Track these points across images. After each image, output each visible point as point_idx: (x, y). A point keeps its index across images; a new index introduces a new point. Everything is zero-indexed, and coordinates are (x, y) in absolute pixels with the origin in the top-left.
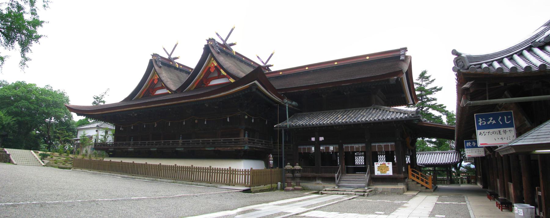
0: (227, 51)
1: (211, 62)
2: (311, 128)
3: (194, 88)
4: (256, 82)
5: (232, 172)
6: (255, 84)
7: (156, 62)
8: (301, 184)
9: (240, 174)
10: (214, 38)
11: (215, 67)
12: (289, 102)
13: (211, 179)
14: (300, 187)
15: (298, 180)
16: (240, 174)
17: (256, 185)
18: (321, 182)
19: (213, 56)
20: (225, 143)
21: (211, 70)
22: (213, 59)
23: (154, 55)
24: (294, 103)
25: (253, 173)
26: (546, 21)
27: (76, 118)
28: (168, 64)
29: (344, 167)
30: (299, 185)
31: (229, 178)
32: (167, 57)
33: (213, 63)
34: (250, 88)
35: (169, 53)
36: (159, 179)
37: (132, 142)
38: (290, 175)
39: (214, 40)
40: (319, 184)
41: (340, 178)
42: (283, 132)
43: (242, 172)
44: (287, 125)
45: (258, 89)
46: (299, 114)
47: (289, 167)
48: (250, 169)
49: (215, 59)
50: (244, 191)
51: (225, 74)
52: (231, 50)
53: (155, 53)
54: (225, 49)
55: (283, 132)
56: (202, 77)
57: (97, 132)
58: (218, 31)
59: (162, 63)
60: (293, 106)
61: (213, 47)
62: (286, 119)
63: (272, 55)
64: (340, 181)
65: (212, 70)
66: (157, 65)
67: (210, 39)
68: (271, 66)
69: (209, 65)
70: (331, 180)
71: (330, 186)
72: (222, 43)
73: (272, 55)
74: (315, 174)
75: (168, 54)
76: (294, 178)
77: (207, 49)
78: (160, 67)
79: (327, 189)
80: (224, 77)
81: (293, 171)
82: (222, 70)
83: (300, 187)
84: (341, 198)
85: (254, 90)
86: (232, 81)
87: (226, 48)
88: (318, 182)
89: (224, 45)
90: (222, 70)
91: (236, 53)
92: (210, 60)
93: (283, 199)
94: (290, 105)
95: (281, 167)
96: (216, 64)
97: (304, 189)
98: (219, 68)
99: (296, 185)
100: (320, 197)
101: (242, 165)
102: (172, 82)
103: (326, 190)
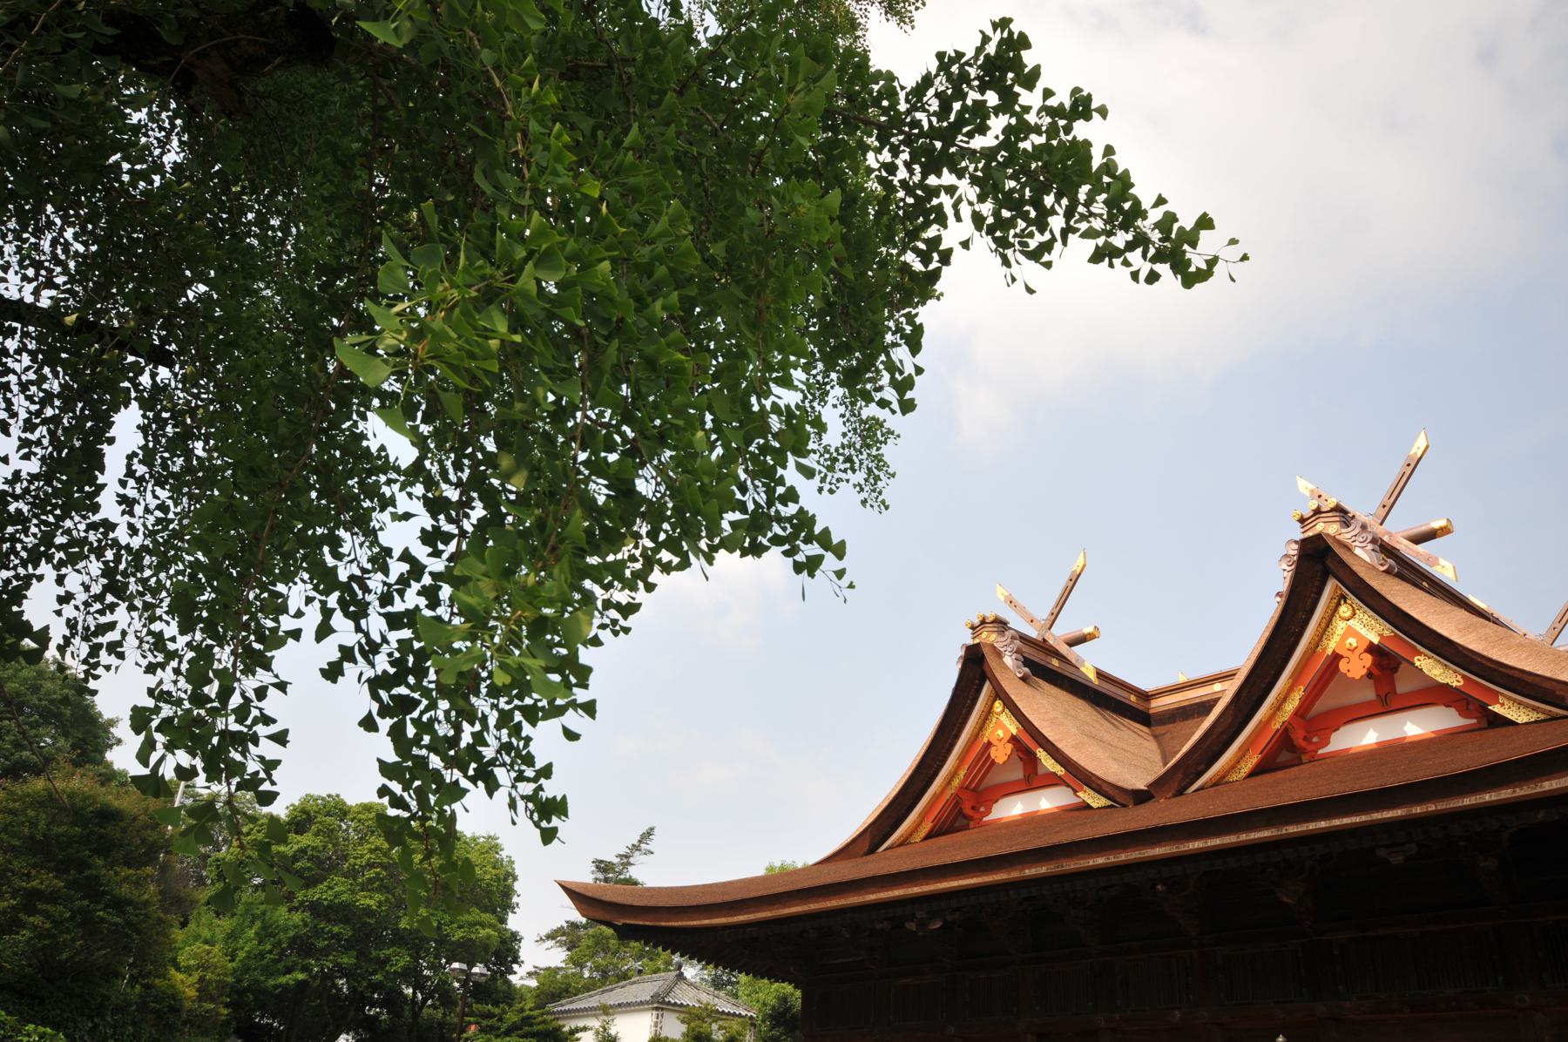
3: (923, 832)
19: (1000, 694)
21: (993, 752)
22: (998, 706)
26: (1558, 609)
33: (1000, 725)
51: (1059, 770)
63: (1074, 580)
65: (1001, 753)
68: (1082, 107)
69: (1331, 645)
72: (1032, 633)
73: (1074, 580)
77: (975, 666)
80: (1052, 781)
82: (1041, 754)
86: (1096, 801)
90: (1041, 754)
91: (1100, 674)
92: (988, 712)
98: (1028, 741)
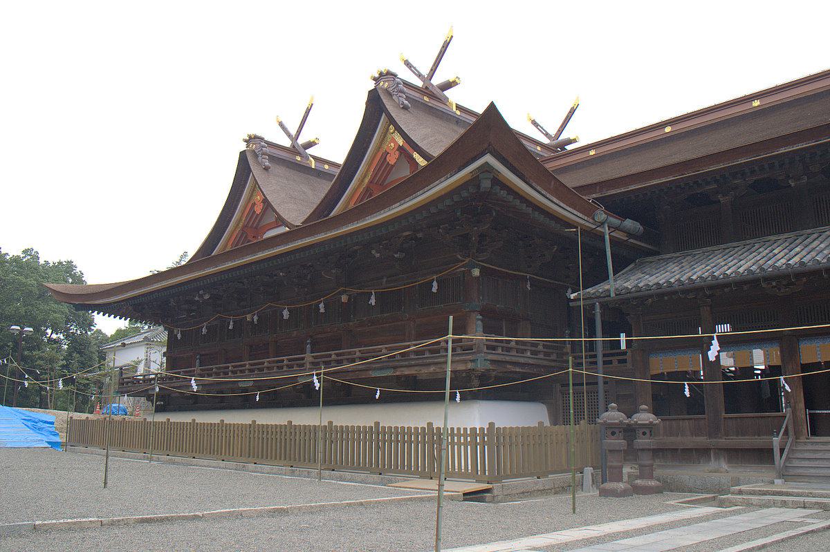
0: (434, 103)
1: (389, 136)
2: (686, 291)
4: (488, 158)
5: (433, 437)
6: (486, 168)
7: (255, 155)
8: (658, 472)
9: (459, 444)
10: (393, 70)
11: (401, 149)
12: (615, 221)
13: (380, 458)
14: (652, 483)
15: (646, 460)
16: (459, 444)
17: (499, 476)
18: (724, 466)
19: (392, 121)
20: (423, 352)
22: (392, 128)
23: (251, 139)
24: (629, 223)
25: (493, 436)
27: (108, 325)
28: (292, 159)
29: (803, 413)
30: (651, 477)
31: (430, 454)
32: (287, 143)
33: (393, 140)
34: (474, 180)
35: (293, 132)
36: (251, 466)
37: (197, 369)
38: (619, 442)
39: (395, 76)
40: (719, 470)
41: (791, 451)
42: (598, 310)
43: (465, 435)
44: (608, 291)
45: (497, 181)
46: (650, 259)
47: (613, 415)
48: (486, 426)
49: (399, 129)
50: (470, 496)
52: (444, 101)
53: (253, 132)
54: (430, 99)
55: (598, 310)
56: (367, 181)
57: (145, 354)
58: (405, 53)
59: (272, 158)
60: (630, 234)
61: (390, 95)
62: (607, 278)
64: (788, 459)
66: (259, 164)
67: (381, 74)
70: (763, 455)
71: (754, 478)
74: (702, 440)
75: (289, 135)
76: (631, 453)
77: (375, 105)
78: (266, 169)
79: (743, 488)
81: (630, 432)
82: (416, 156)
83: (652, 483)
84: (793, 525)
85: (486, 184)
87: (432, 96)
88: (713, 464)
89: (426, 91)
90: (416, 156)
91: (458, 107)
93: (143, 295)
94: (617, 228)
95: (593, 418)
96: (401, 142)
97: (667, 487)
98: (407, 147)
99: (641, 477)
100: (715, 516)
101: (475, 416)
102: (293, 204)
103: (740, 492)
